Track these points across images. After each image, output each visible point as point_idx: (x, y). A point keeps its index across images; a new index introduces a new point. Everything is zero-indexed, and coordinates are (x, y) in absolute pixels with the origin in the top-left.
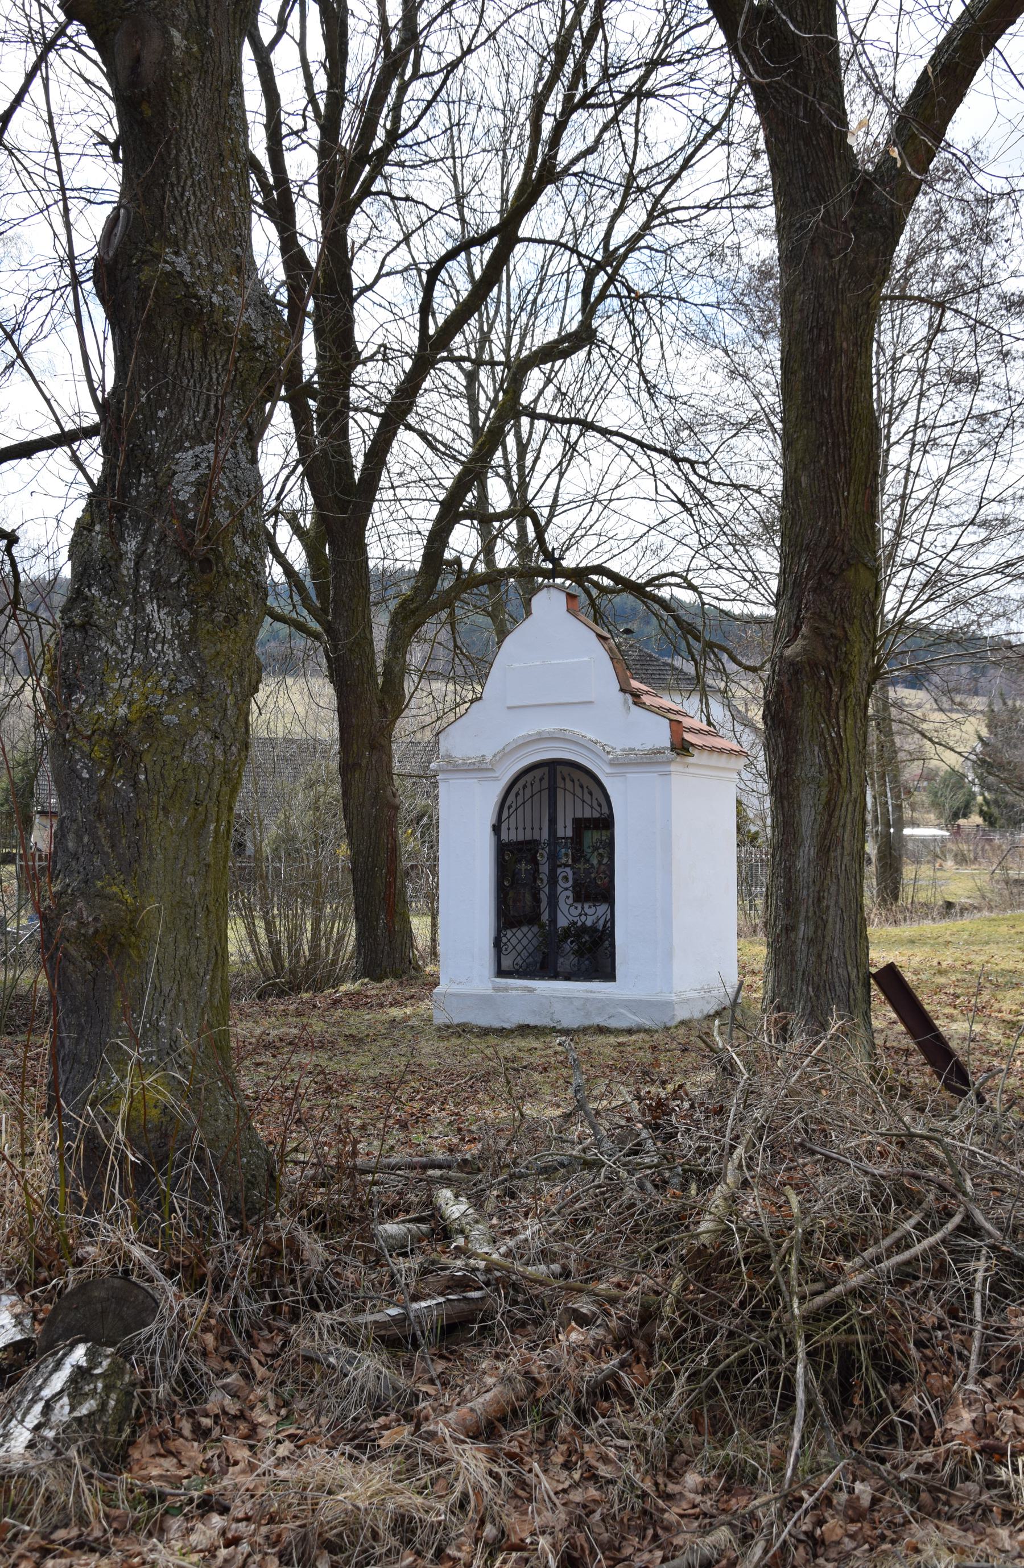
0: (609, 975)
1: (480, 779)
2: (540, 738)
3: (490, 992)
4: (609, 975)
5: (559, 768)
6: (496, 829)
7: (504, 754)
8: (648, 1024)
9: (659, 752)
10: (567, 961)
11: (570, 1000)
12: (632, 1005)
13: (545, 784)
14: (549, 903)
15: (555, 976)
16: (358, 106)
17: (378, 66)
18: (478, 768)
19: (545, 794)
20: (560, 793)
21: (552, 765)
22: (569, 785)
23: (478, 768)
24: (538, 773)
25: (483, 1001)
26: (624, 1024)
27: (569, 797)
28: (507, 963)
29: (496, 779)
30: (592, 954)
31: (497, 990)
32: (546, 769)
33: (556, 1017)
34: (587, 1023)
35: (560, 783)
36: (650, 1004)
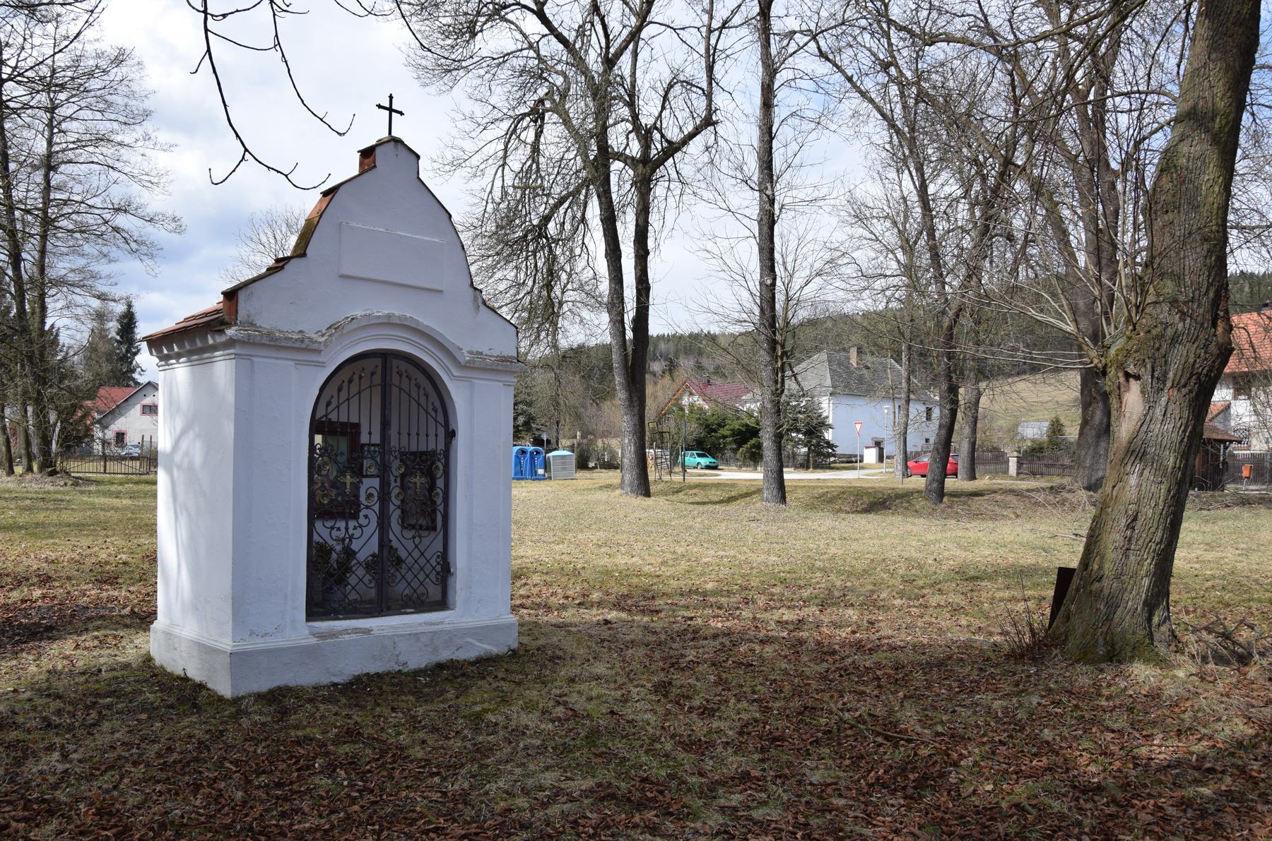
1: (298, 362)
2: (389, 323)
3: (314, 641)
4: (442, 604)
5: (395, 362)
8: (495, 650)
11: (416, 636)
13: (378, 379)
18: (301, 347)
20: (395, 391)
21: (385, 356)
23: (301, 347)
25: (305, 653)
28: (434, 592)
29: (322, 365)
31: (322, 636)
32: (378, 361)
33: (402, 659)
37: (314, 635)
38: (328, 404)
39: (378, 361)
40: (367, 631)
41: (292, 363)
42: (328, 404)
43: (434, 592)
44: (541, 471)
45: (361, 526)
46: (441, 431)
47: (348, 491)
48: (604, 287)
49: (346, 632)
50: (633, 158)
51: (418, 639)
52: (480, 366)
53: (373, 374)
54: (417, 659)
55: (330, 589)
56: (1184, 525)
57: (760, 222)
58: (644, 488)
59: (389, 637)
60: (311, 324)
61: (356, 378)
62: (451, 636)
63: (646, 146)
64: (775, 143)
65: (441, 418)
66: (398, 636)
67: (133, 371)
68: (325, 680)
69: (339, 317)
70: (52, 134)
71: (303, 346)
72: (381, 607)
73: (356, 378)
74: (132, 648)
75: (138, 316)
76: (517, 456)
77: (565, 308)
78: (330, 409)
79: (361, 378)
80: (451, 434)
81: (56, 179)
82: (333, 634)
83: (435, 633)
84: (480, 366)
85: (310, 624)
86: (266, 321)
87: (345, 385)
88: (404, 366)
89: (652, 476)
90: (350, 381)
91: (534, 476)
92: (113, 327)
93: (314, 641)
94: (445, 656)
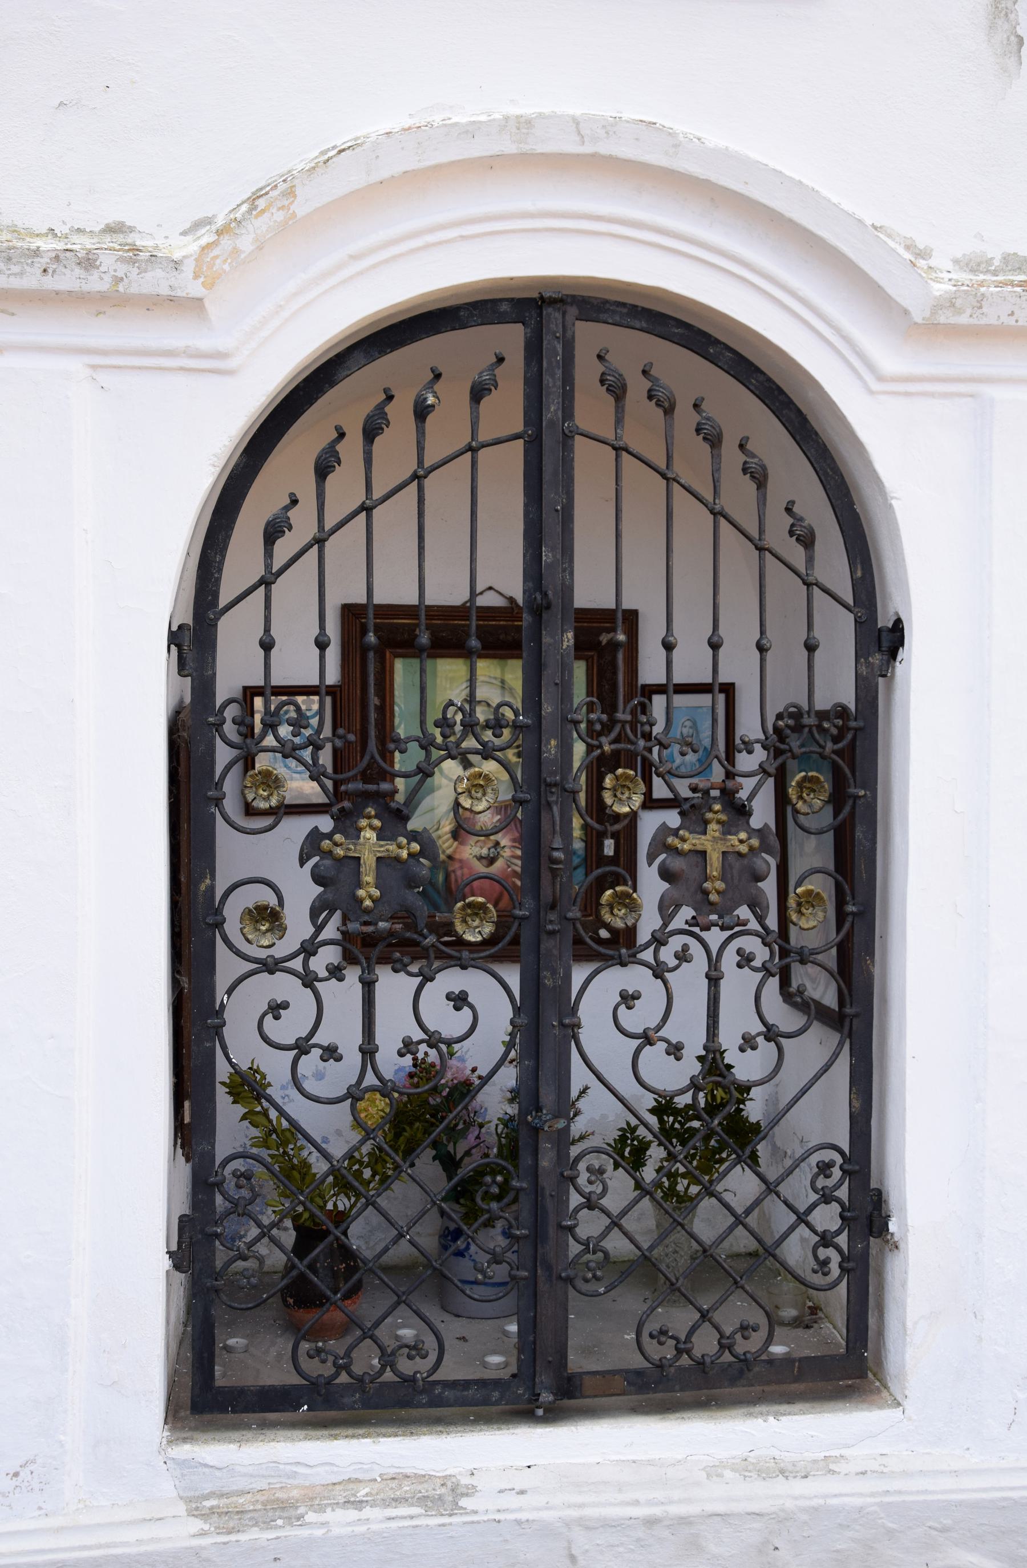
0: (848, 1367)
2: (524, 158)
4: (848, 1367)
5: (589, 337)
6: (193, 643)
10: (601, 1334)
13: (506, 409)
15: (544, 1389)
19: (505, 470)
20: (590, 467)
21: (542, 313)
22: (643, 429)
24: (462, 351)
27: (644, 488)
29: (215, 365)
32: (511, 338)
35: (591, 409)
37: (196, 1512)
38: (274, 531)
39: (511, 338)
40: (446, 1496)
41: (76, 365)
42: (274, 531)
45: (771, 1034)
46: (839, 632)
47: (368, 892)
49: (347, 1494)
51: (694, 1546)
53: (478, 393)
59: (545, 1531)
61: (401, 412)
65: (834, 568)
66: (587, 1525)
71: (96, 283)
73: (401, 412)
78: (284, 548)
79: (421, 412)
82: (280, 1507)
83: (782, 1519)
85: (186, 1451)
87: (351, 449)
88: (631, 349)
90: (371, 431)
93: (182, 1532)
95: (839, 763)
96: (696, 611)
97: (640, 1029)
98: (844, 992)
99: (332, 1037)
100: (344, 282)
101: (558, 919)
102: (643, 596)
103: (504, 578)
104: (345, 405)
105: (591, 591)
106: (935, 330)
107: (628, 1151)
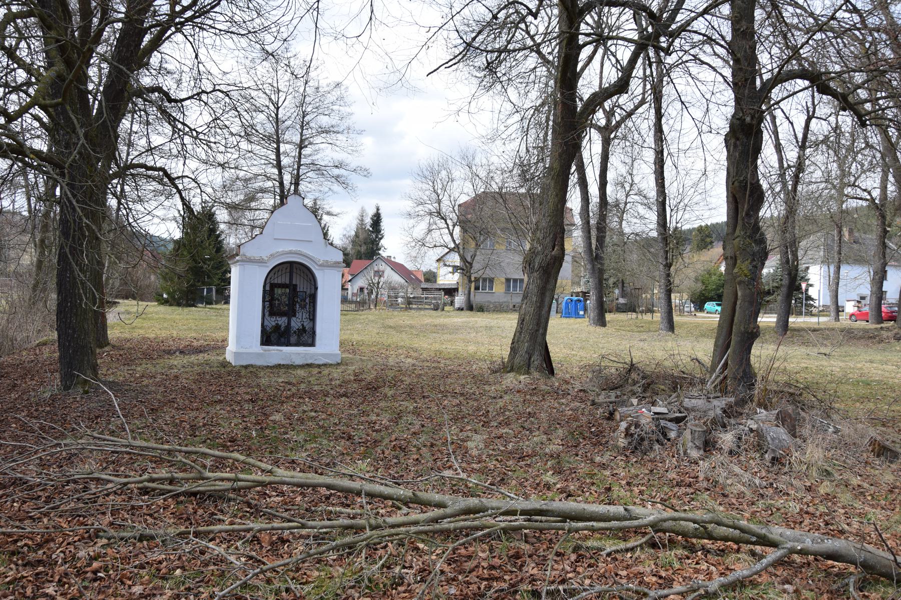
0: (312, 344)
2: (290, 253)
4: (312, 344)
7: (272, 256)
9: (339, 263)
10: (293, 339)
12: (324, 355)
13: (288, 270)
14: (605, 521)
15: (288, 344)
16: (713, 518)
17: (550, 137)
19: (288, 275)
20: (294, 275)
21: (291, 263)
22: (298, 272)
24: (285, 266)
26: (321, 363)
30: (307, 337)
34: (306, 362)
35: (295, 270)
36: (331, 355)
43: (310, 341)
44: (582, 313)
48: (653, 194)
50: (600, 127)
52: (326, 265)
54: (299, 361)
55: (269, 337)
56: (550, 322)
57: (655, 163)
58: (601, 322)
60: (265, 255)
62: (313, 355)
63: (609, 121)
64: (663, 120)
67: (380, 249)
68: (265, 364)
69: (274, 252)
70: (302, 130)
72: (297, 344)
74: (212, 357)
75: (383, 216)
76: (566, 303)
77: (628, 206)
80: (316, 288)
81: (304, 152)
84: (326, 265)
86: (248, 255)
88: (298, 266)
89: (676, 318)
91: (577, 316)
92: (368, 221)
94: (309, 362)
95: (313, 298)
96: (302, 286)
97: (296, 324)
98: (313, 318)
99: (271, 322)
100: (199, 350)
101: (291, 313)
102: (298, 283)
103: (288, 282)
104: (276, 269)
105: (294, 283)
106: (320, 266)
107: (295, 332)
